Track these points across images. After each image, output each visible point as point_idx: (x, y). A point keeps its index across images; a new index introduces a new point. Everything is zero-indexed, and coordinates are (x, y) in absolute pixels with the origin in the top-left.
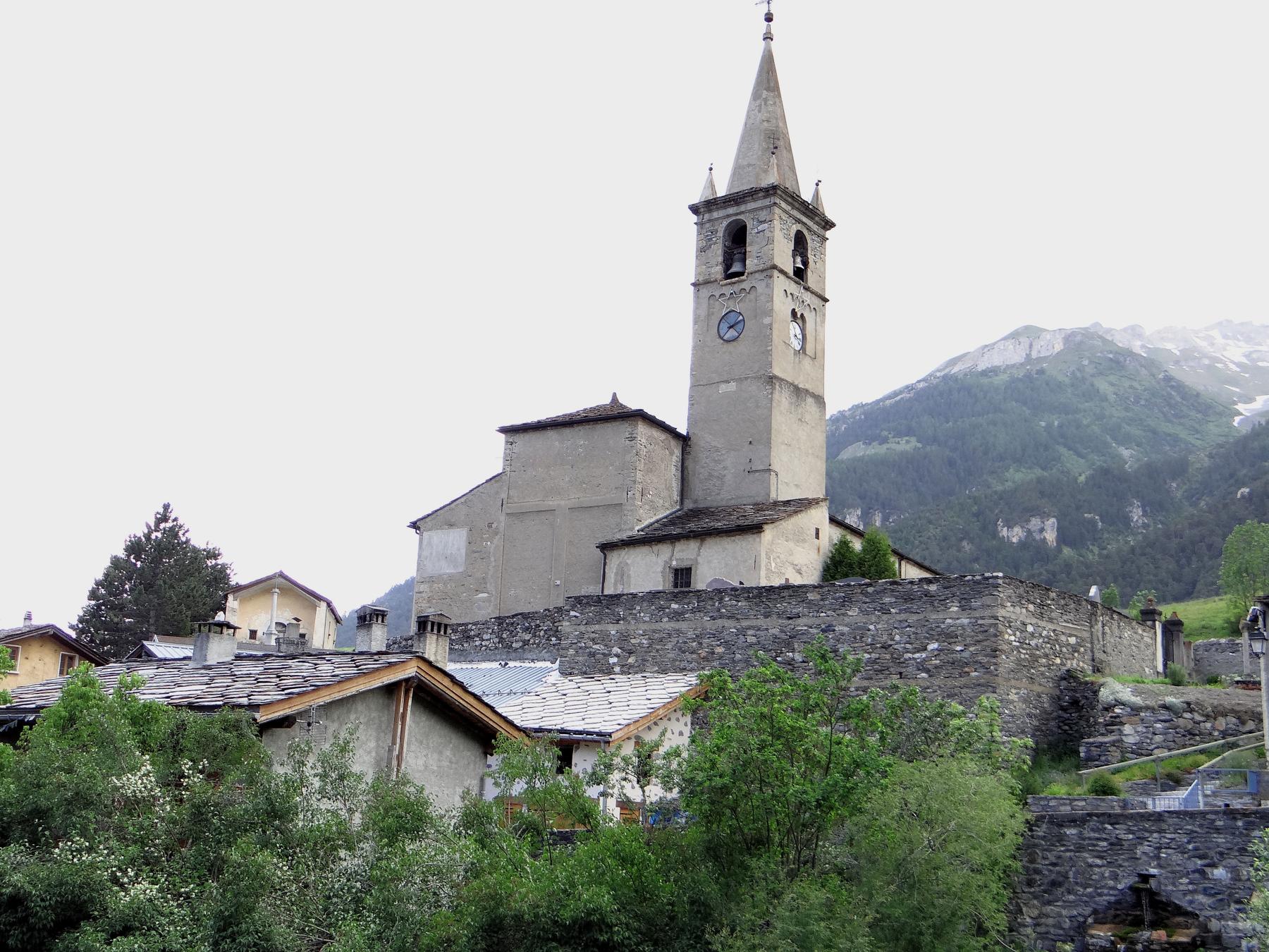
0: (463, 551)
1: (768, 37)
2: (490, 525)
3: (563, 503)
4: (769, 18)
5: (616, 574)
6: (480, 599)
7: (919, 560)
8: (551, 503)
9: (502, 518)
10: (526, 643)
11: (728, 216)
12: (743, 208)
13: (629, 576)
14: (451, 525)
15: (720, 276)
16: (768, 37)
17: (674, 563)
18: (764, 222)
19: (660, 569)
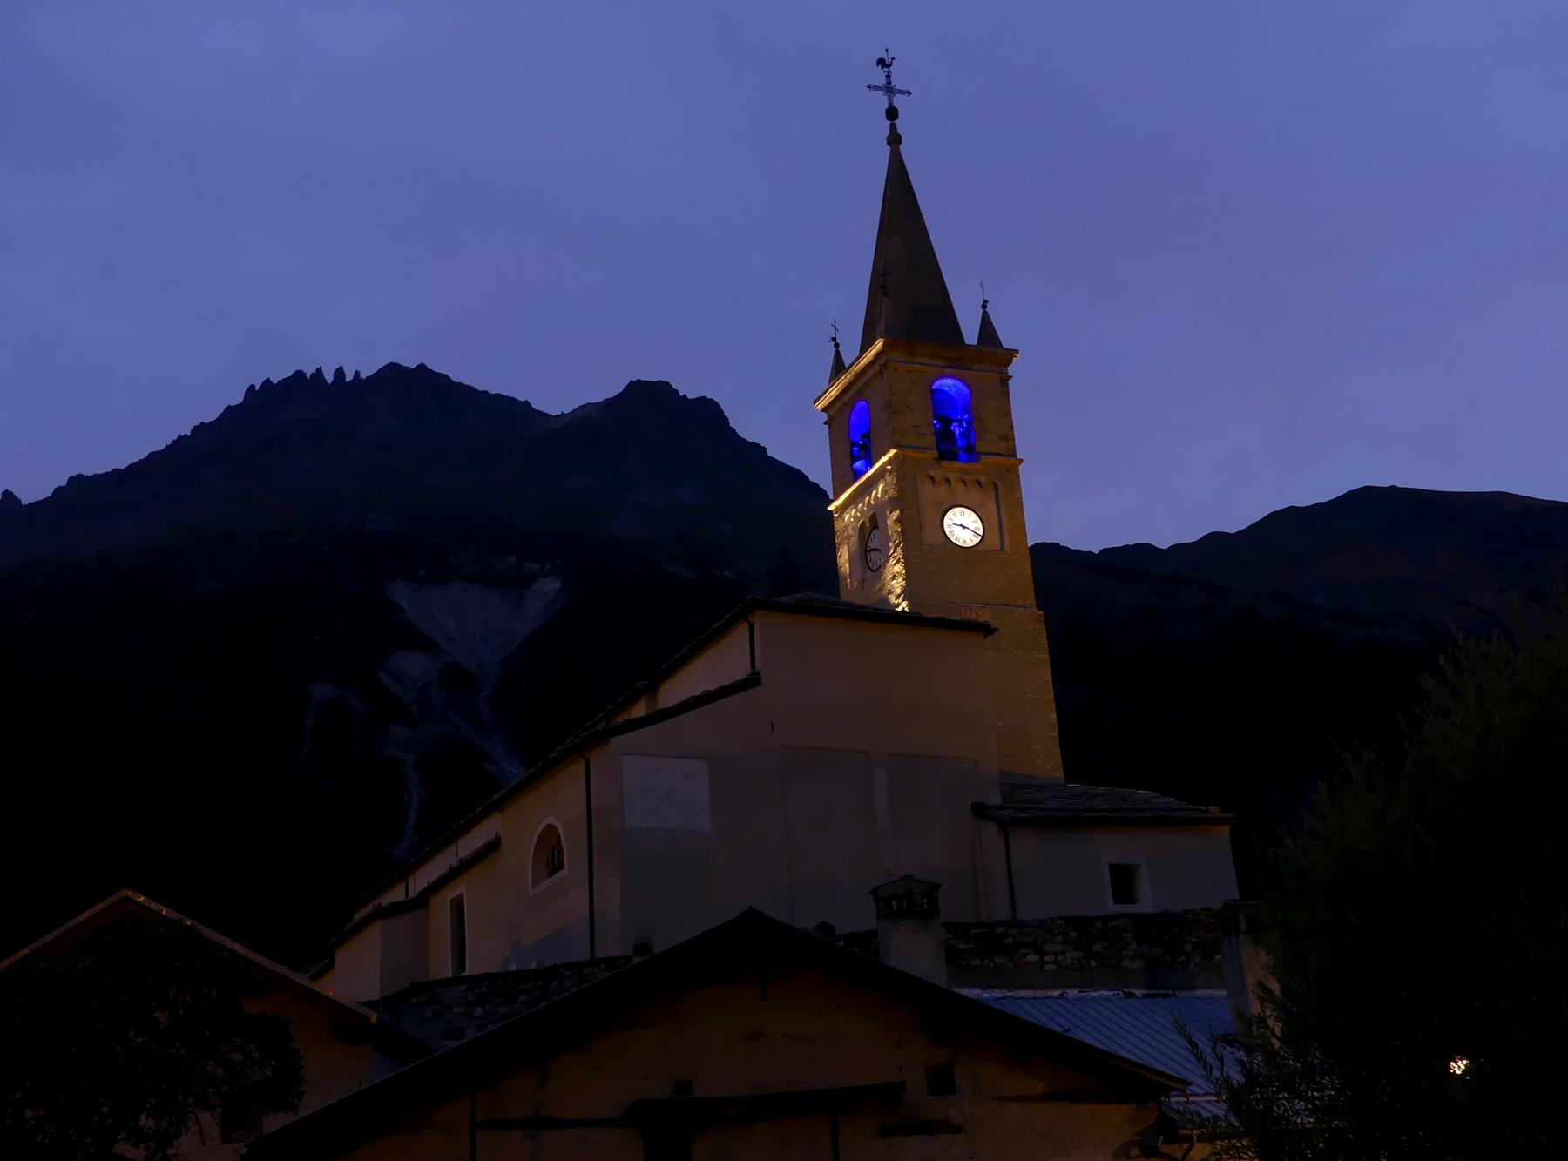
1: (894, 139)
4: (892, 114)
16: (894, 139)
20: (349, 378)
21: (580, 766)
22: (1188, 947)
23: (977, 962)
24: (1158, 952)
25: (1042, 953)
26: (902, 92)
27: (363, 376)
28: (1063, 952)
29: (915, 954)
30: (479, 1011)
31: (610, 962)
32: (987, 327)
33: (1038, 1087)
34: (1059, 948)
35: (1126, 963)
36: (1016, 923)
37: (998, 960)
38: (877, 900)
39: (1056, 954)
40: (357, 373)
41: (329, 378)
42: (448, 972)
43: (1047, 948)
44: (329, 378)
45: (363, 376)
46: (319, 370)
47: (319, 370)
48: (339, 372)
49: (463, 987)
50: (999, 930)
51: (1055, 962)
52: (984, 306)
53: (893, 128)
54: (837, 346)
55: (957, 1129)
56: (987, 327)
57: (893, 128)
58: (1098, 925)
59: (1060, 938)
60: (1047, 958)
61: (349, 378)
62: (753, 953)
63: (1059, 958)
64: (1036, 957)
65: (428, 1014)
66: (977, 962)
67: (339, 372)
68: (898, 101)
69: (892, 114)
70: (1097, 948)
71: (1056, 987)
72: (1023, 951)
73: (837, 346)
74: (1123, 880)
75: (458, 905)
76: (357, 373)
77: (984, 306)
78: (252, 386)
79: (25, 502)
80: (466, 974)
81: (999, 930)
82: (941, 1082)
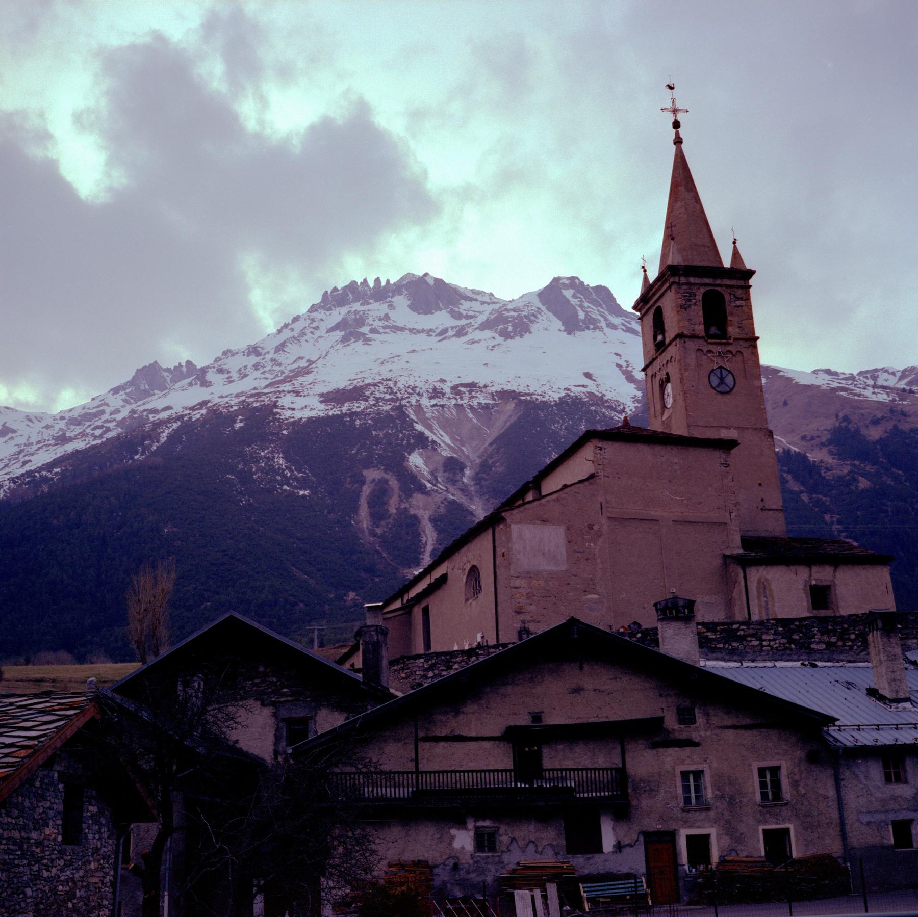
0: (563, 550)
1: (678, 141)
2: (590, 527)
3: (665, 514)
4: (676, 125)
5: (758, 588)
6: (590, 600)
7: (499, 600)
8: (655, 513)
9: (604, 521)
10: (829, 645)
11: (706, 285)
12: (718, 282)
13: (771, 590)
14: (544, 521)
15: (703, 334)
16: (678, 141)
17: (814, 582)
18: (741, 299)
19: (801, 586)
20: (383, 283)
21: (490, 531)
22: (853, 637)
23: (721, 646)
24: (833, 639)
25: (761, 640)
26: (683, 111)
27: (392, 282)
28: (774, 640)
29: (678, 643)
30: (431, 674)
31: (504, 645)
32: (736, 254)
33: (747, 721)
34: (771, 637)
35: (814, 646)
36: (748, 623)
37: (734, 644)
38: (657, 610)
39: (770, 641)
40: (388, 281)
41: (371, 284)
42: (422, 651)
43: (764, 637)
44: (371, 284)
45: (392, 282)
46: (365, 280)
47: (365, 280)
48: (377, 280)
49: (422, 660)
50: (735, 627)
51: (769, 645)
52: (734, 243)
53: (677, 134)
54: (645, 271)
55: (697, 745)
56: (736, 254)
57: (677, 134)
58: (797, 623)
59: (772, 631)
60: (764, 643)
61: (383, 283)
62: (571, 646)
63: (772, 643)
64: (758, 643)
65: (403, 675)
66: (721, 646)
67: (377, 280)
68: (681, 117)
69: (676, 125)
70: (796, 637)
71: (770, 661)
72: (749, 639)
73: (645, 271)
74: (820, 595)
75: (426, 611)
76: (388, 281)
77: (734, 243)
78: (326, 292)
79: (199, 367)
80: (432, 651)
81: (735, 627)
82: (686, 717)
